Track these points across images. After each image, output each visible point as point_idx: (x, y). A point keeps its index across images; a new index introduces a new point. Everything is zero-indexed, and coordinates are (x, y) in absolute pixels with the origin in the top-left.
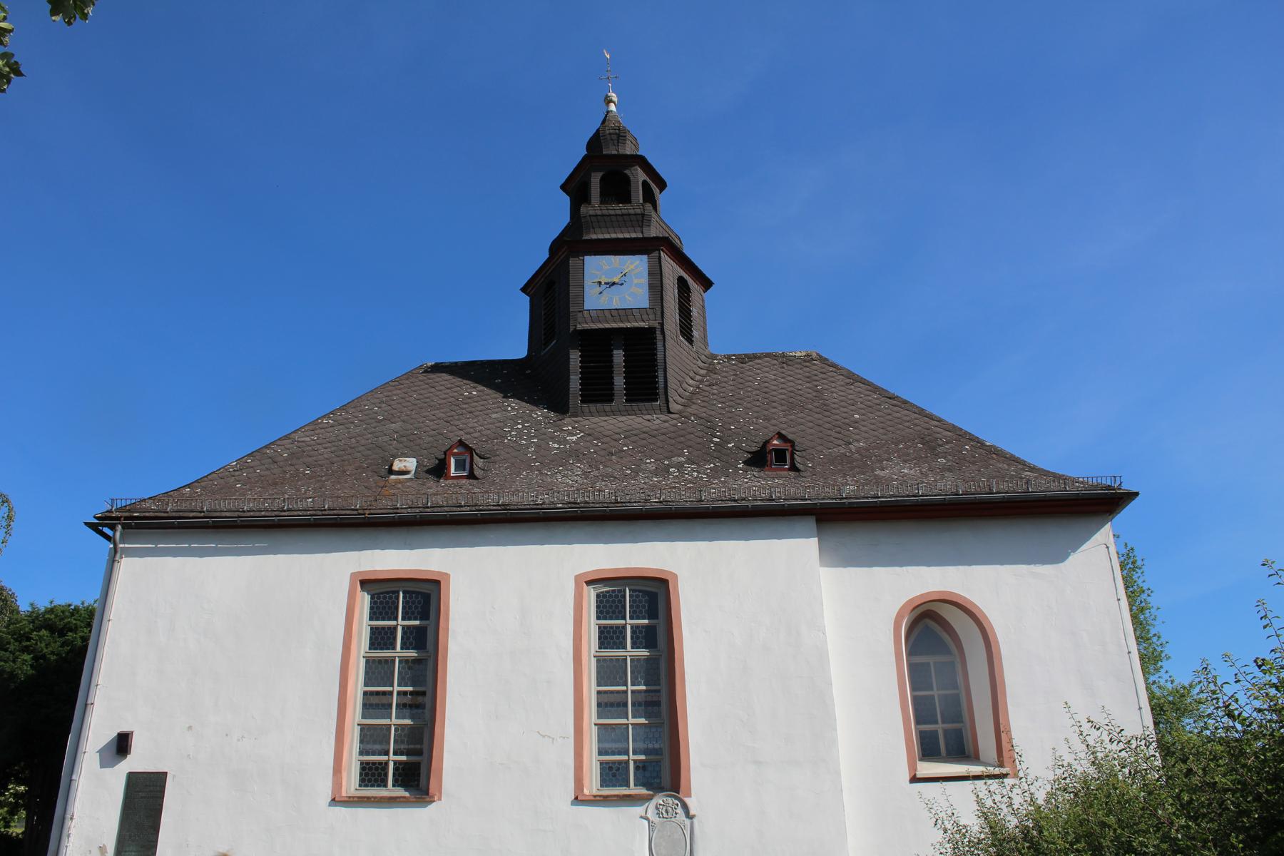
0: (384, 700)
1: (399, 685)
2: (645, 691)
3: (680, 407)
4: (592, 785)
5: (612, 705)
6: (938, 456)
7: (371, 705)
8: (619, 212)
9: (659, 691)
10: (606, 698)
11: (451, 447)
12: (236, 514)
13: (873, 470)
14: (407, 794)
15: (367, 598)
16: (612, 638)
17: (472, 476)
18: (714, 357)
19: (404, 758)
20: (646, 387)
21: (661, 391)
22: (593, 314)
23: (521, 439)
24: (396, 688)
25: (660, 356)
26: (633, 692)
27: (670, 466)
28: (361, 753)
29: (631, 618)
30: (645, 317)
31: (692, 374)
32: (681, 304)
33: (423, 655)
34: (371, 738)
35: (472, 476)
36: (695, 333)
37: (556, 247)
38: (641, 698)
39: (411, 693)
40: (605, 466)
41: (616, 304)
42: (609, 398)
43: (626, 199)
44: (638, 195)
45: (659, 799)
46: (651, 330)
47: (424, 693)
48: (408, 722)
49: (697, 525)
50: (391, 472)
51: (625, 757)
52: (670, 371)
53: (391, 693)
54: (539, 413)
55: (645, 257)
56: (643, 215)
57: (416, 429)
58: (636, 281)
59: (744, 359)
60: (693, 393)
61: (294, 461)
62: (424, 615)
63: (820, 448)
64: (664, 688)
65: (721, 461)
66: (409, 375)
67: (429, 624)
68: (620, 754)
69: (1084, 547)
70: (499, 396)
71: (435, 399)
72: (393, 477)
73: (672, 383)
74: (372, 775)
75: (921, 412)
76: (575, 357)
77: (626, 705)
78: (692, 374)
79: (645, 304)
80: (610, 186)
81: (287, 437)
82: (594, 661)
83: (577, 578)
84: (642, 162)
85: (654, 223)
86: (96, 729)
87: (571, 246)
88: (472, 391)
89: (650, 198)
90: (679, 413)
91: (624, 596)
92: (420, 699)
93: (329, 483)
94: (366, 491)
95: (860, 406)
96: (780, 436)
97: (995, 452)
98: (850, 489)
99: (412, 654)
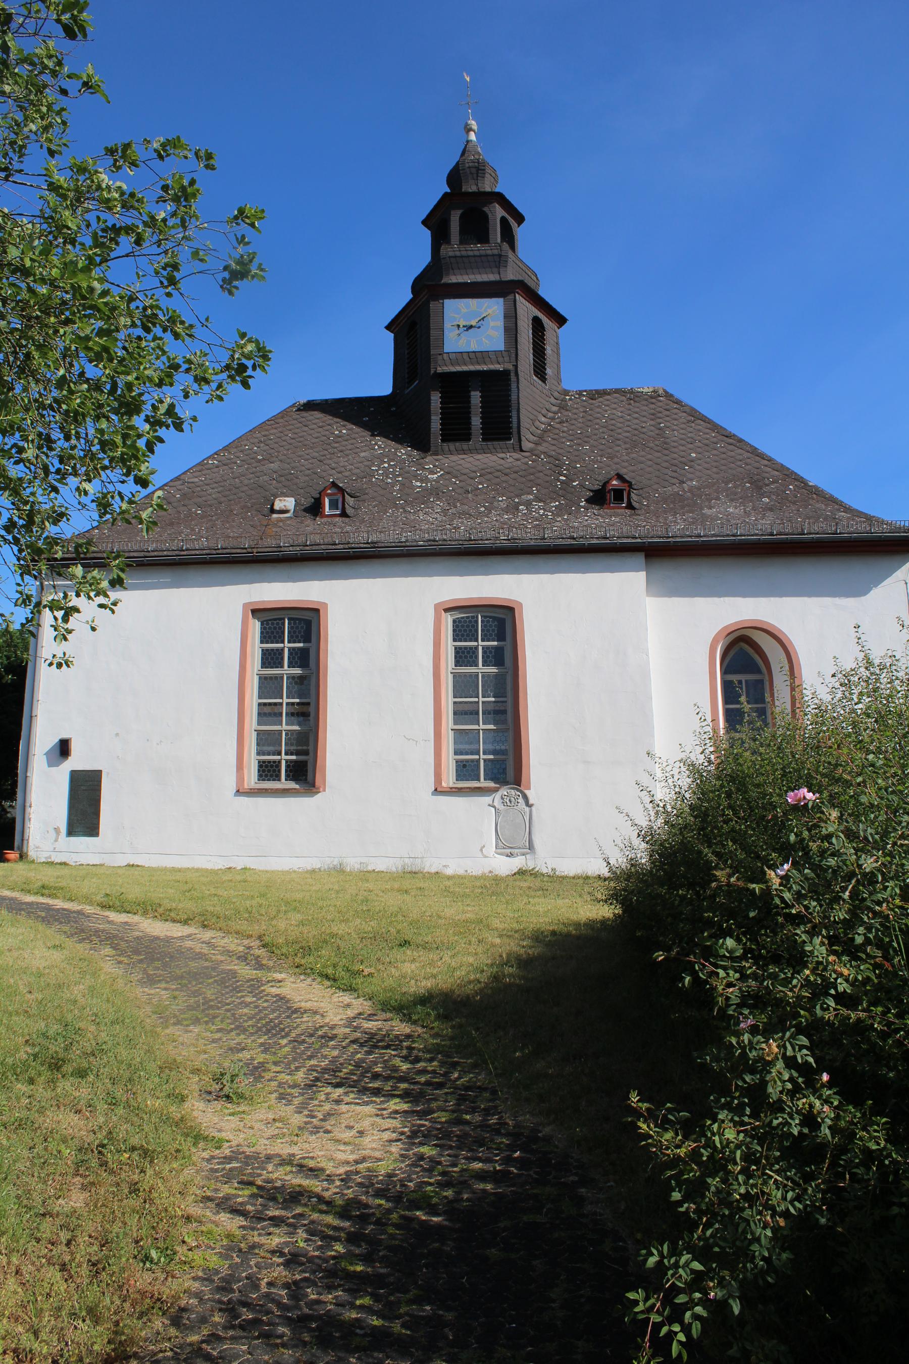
0: (276, 709)
1: (288, 697)
2: (494, 702)
3: (531, 445)
4: (449, 779)
5: (466, 713)
6: (763, 495)
7: (265, 714)
8: (477, 253)
9: (506, 702)
10: (461, 708)
11: (325, 489)
12: (142, 554)
13: (702, 509)
14: (297, 786)
15: (258, 624)
16: (466, 657)
17: (344, 514)
18: (566, 392)
19: (294, 757)
20: (500, 427)
21: (515, 430)
22: (452, 356)
23: (388, 477)
24: (285, 700)
25: (514, 397)
26: (483, 702)
27: (519, 504)
28: (258, 754)
29: (483, 640)
30: (500, 359)
31: (544, 411)
32: (535, 344)
33: (307, 672)
34: (266, 740)
35: (344, 514)
36: (549, 371)
37: (419, 285)
38: (490, 708)
39: (298, 704)
40: (462, 504)
41: (474, 347)
42: (467, 437)
43: (483, 237)
44: (496, 234)
45: (504, 791)
46: (505, 374)
47: (308, 704)
48: (297, 728)
49: (540, 560)
50: (272, 511)
51: (477, 757)
52: (522, 411)
53: (281, 704)
54: (403, 452)
55: (501, 300)
56: (500, 256)
57: (293, 468)
58: (492, 324)
59: (595, 395)
60: (544, 431)
61: (187, 502)
62: (307, 638)
63: (655, 487)
64: (510, 699)
65: (565, 499)
66: (284, 414)
67: (312, 646)
68: (472, 754)
69: (883, 584)
70: (367, 434)
71: (309, 438)
72: (275, 516)
73: (525, 422)
74: (268, 771)
75: (754, 451)
76: (436, 399)
77: (477, 713)
78: (544, 411)
79: (501, 347)
80: (470, 219)
81: (178, 478)
82: (450, 677)
83: (437, 606)
84: (501, 199)
85: (510, 263)
86: (41, 735)
87: (430, 288)
88: (342, 429)
89: (508, 236)
90: (531, 451)
91: (477, 622)
92: (304, 709)
93: (218, 522)
94: (251, 529)
95: (698, 444)
96: (619, 477)
97: (817, 492)
98: (678, 527)
99: (298, 671)
